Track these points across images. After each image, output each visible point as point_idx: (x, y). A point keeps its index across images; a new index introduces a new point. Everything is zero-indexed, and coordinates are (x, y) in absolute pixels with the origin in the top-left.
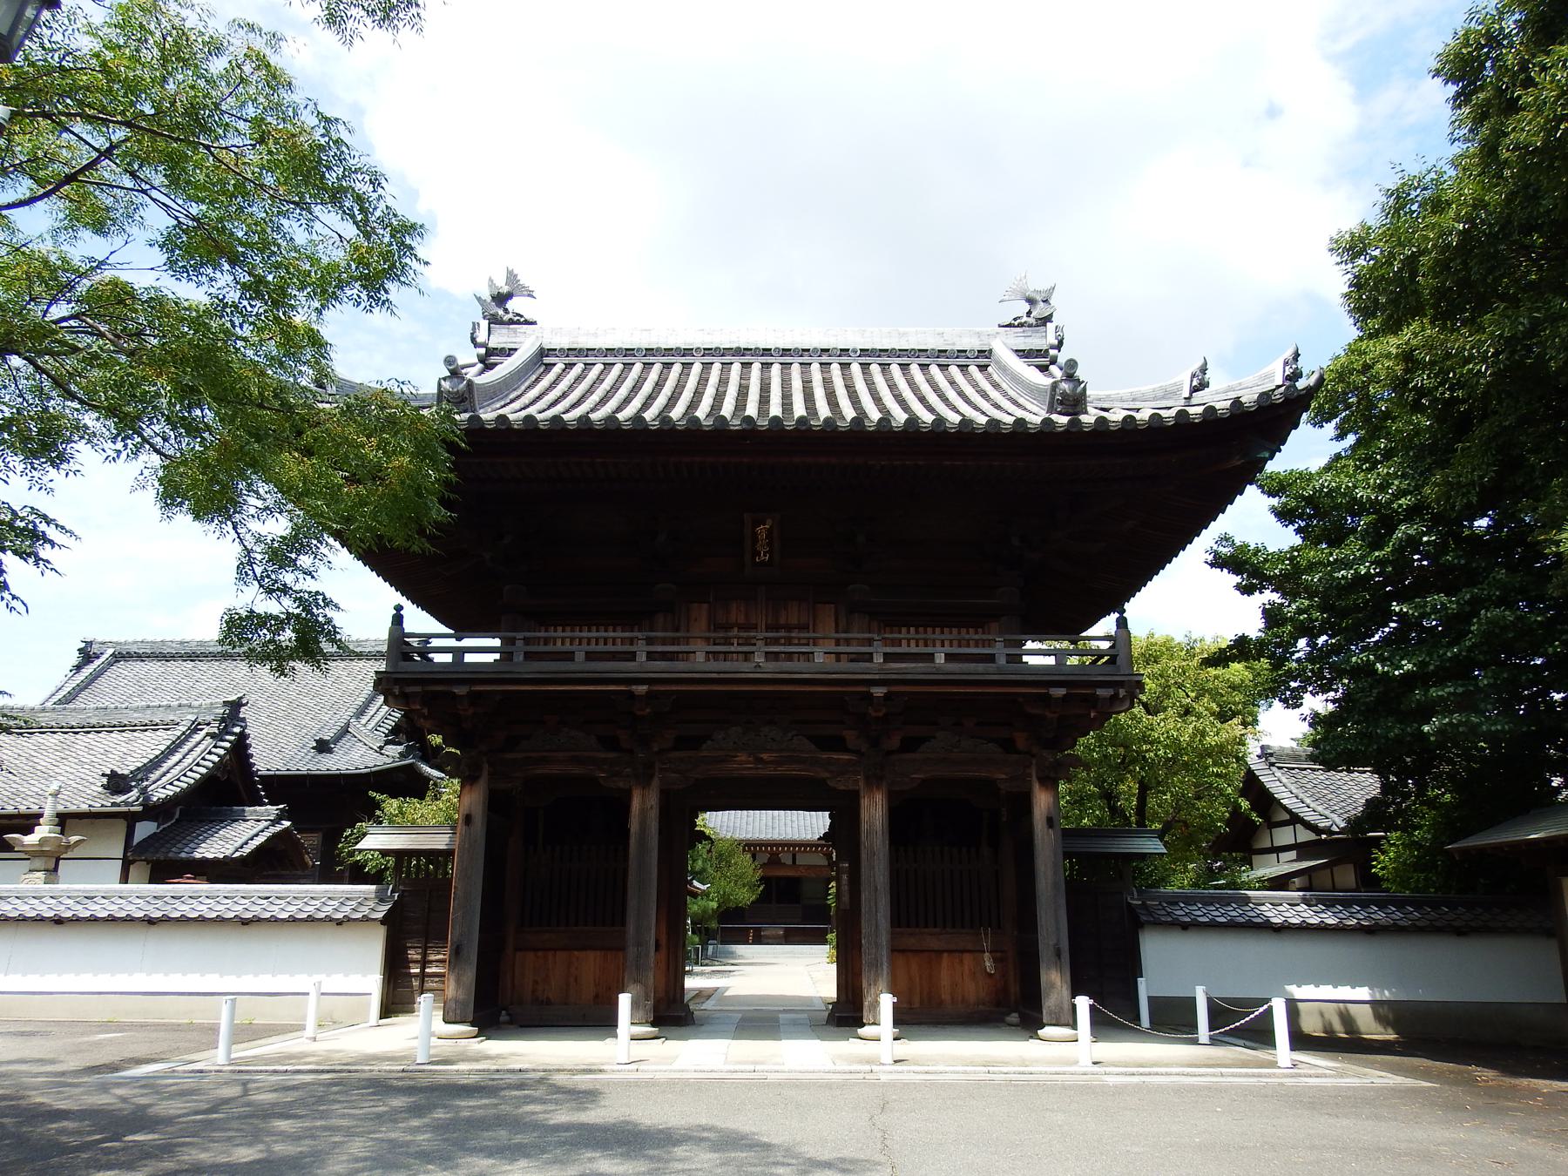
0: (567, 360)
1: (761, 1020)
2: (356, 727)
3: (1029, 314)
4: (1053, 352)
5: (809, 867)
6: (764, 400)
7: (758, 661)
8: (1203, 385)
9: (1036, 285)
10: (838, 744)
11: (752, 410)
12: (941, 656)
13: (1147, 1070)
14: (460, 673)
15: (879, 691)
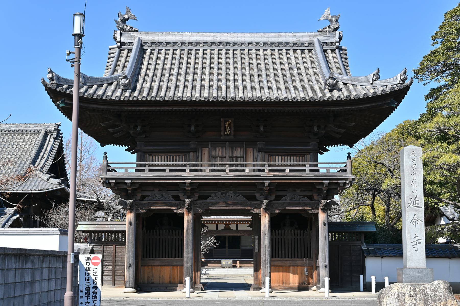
0: (151, 48)
8: (378, 79)
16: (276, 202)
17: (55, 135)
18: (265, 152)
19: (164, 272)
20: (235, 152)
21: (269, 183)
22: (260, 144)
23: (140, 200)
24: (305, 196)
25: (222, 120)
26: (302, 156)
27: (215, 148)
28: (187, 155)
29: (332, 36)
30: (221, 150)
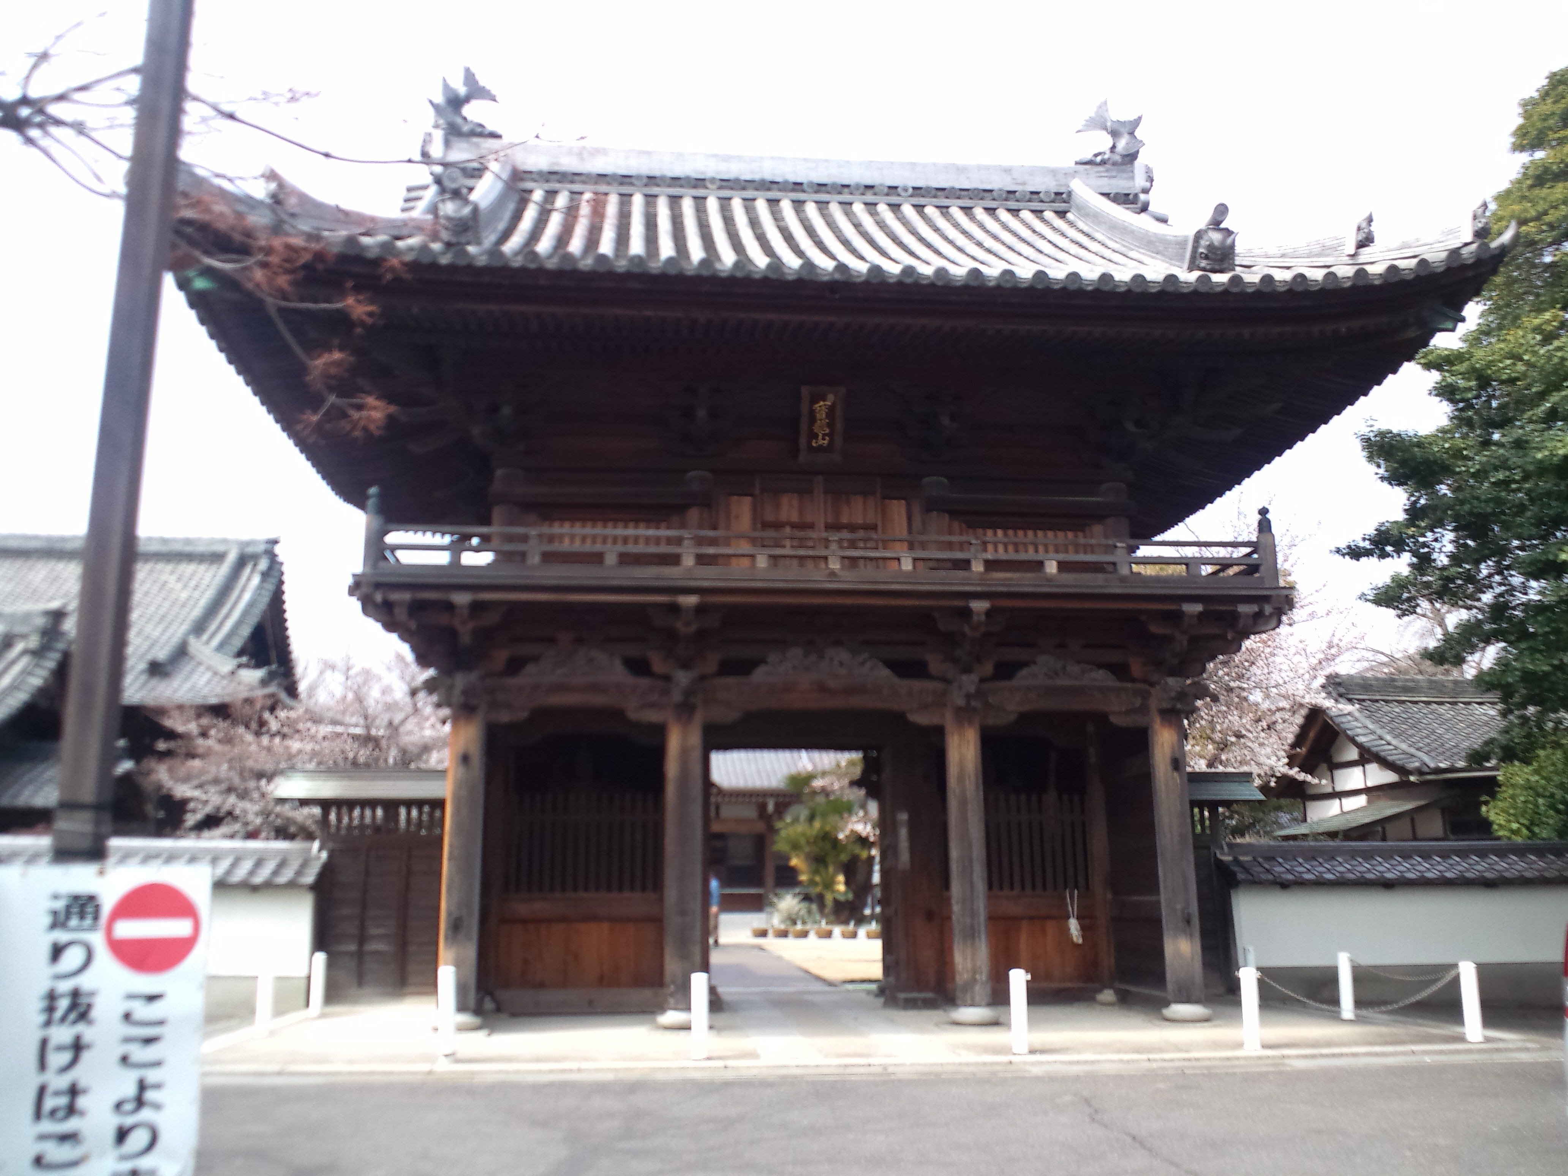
1: (805, 1003)
2: (196, 645)
3: (1113, 147)
4: (1142, 197)
5: (739, 821)
6: (623, 238)
7: (833, 569)
9: (1119, 114)
11: (606, 247)
12: (1051, 562)
13: (1336, 1050)
17: (263, 564)
21: (988, 613)
22: (935, 484)
24: (1100, 666)
25: (805, 391)
29: (1125, 175)
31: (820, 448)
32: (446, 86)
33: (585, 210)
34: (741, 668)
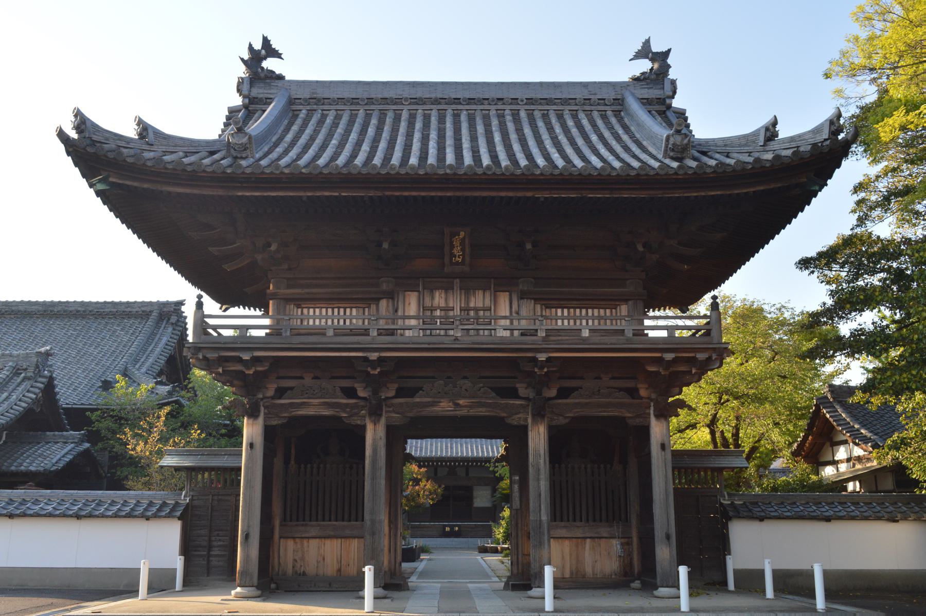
10: (513, 393)
14: (243, 341)
15: (542, 357)
16: (560, 401)
18: (536, 300)
19: (321, 552)
20: (473, 299)
23: (273, 398)
24: (620, 389)
26: (611, 309)
27: (432, 291)
28: (373, 307)
30: (443, 295)
31: (457, 263)
32: (251, 47)
33: (329, 121)
34: (411, 392)
